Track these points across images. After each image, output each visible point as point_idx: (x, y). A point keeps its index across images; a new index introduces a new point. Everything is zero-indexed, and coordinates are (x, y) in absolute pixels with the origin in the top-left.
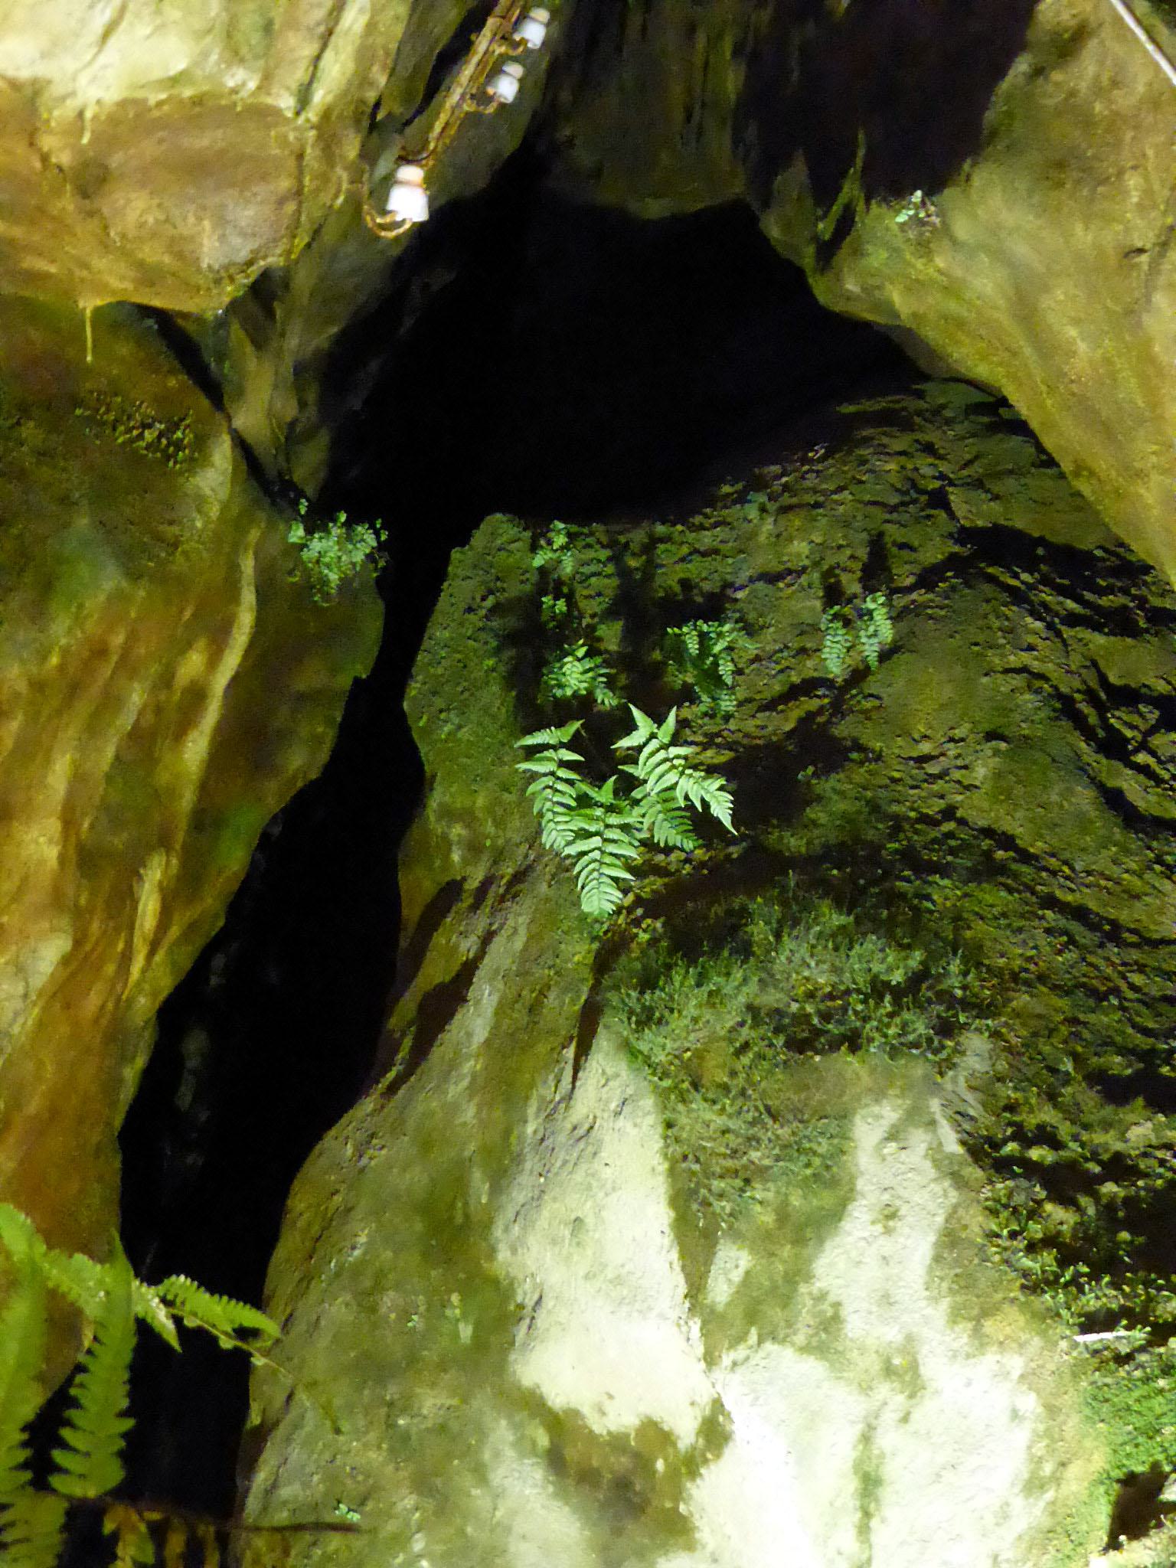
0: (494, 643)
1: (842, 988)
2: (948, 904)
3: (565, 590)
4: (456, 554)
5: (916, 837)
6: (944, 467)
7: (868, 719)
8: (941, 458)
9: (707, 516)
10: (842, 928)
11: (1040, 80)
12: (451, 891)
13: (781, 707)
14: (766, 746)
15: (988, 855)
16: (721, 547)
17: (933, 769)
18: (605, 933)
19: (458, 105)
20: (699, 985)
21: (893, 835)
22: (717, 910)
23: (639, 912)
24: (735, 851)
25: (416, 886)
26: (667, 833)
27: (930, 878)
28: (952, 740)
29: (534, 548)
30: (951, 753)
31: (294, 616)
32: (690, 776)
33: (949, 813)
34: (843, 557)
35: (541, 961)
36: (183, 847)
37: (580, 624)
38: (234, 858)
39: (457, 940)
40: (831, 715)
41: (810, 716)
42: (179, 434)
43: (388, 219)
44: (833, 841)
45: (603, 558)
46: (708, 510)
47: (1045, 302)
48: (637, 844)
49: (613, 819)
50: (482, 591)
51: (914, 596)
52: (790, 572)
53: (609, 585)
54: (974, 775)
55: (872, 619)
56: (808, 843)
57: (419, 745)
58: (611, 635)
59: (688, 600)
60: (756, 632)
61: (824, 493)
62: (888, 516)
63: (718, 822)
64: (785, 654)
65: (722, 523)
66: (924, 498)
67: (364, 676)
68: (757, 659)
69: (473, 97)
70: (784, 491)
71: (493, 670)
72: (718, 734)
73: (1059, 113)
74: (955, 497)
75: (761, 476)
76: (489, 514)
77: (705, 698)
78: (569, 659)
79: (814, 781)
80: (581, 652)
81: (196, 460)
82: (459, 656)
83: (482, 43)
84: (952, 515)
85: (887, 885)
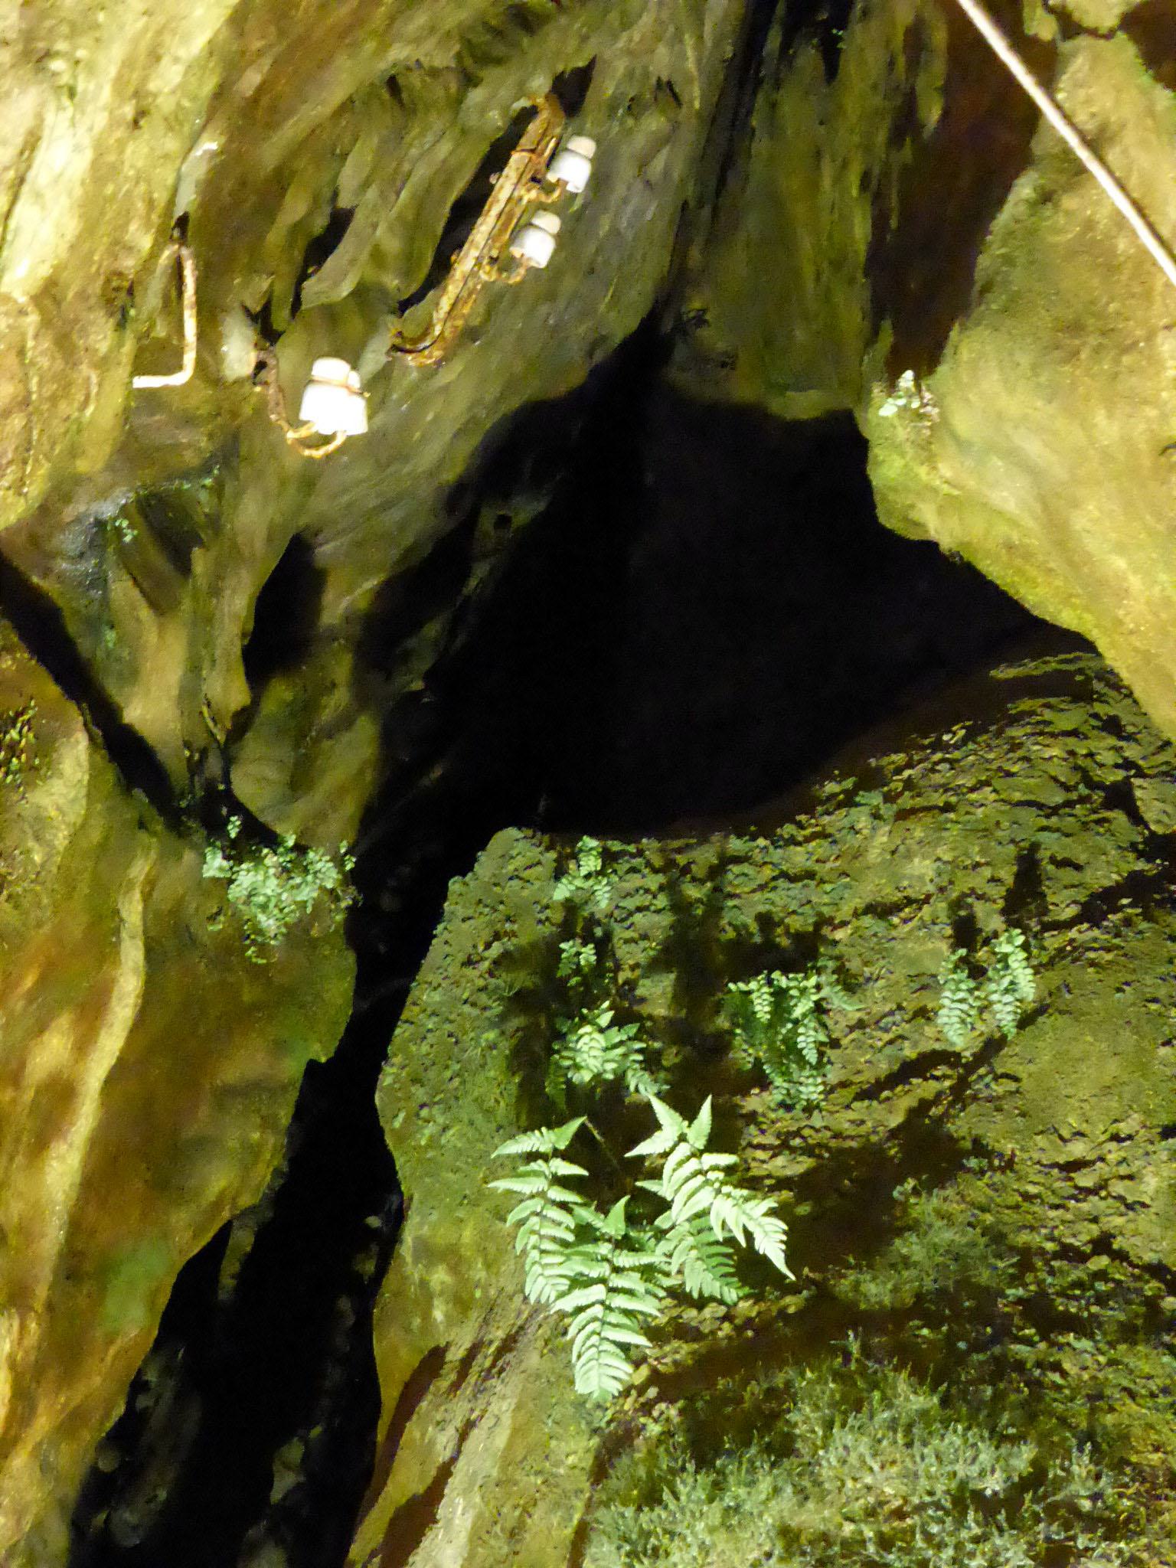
0: (497, 1009)
1: (916, 1500)
2: (1086, 1376)
3: (598, 932)
4: (455, 885)
5: (1049, 1280)
6: (1132, 752)
7: (999, 1109)
8: (1130, 738)
9: (801, 826)
10: (924, 1414)
11: (1048, 210)
12: (435, 1359)
13: (886, 1094)
14: (863, 1148)
15: (1152, 1304)
16: (817, 867)
17: (1085, 1179)
18: (609, 1423)
19: (473, 274)
20: (711, 1500)
21: (1016, 1280)
22: (754, 1390)
23: (652, 1392)
24: (792, 1304)
25: (394, 1354)
26: (701, 1279)
27: (1061, 1339)
28: (1116, 1138)
29: (559, 873)
30: (1112, 1157)
31: (204, 983)
32: (729, 1195)
33: (1103, 1244)
34: (978, 881)
35: (527, 1465)
36: (50, 1307)
37: (615, 979)
38: (131, 1320)
39: (430, 1434)
40: (952, 1105)
41: (924, 1105)
42: (14, 734)
43: (303, 432)
44: (929, 1285)
45: (654, 887)
46: (802, 818)
47: (1079, 522)
48: (662, 1294)
49: (625, 1259)
50: (487, 935)
51: (1073, 933)
52: (909, 901)
53: (658, 923)
54: (1142, 1187)
55: (1007, 967)
56: (896, 1290)
57: (396, 1154)
58: (658, 995)
59: (769, 945)
60: (859, 985)
61: (957, 790)
62: (1044, 822)
63: (765, 1261)
64: (898, 1018)
65: (823, 835)
66: (1098, 796)
67: (323, 1060)
68: (861, 1025)
69: (493, 261)
70: (905, 788)
71: (493, 1046)
72: (797, 1133)
73: (1072, 253)
74: (1144, 793)
75: (879, 769)
76: (501, 829)
77: (779, 1081)
78: (588, 1029)
79: (912, 1200)
80: (605, 1019)
81: (36, 769)
82: (448, 1027)
83: (506, 186)
84: (1136, 818)
85: (997, 1350)
